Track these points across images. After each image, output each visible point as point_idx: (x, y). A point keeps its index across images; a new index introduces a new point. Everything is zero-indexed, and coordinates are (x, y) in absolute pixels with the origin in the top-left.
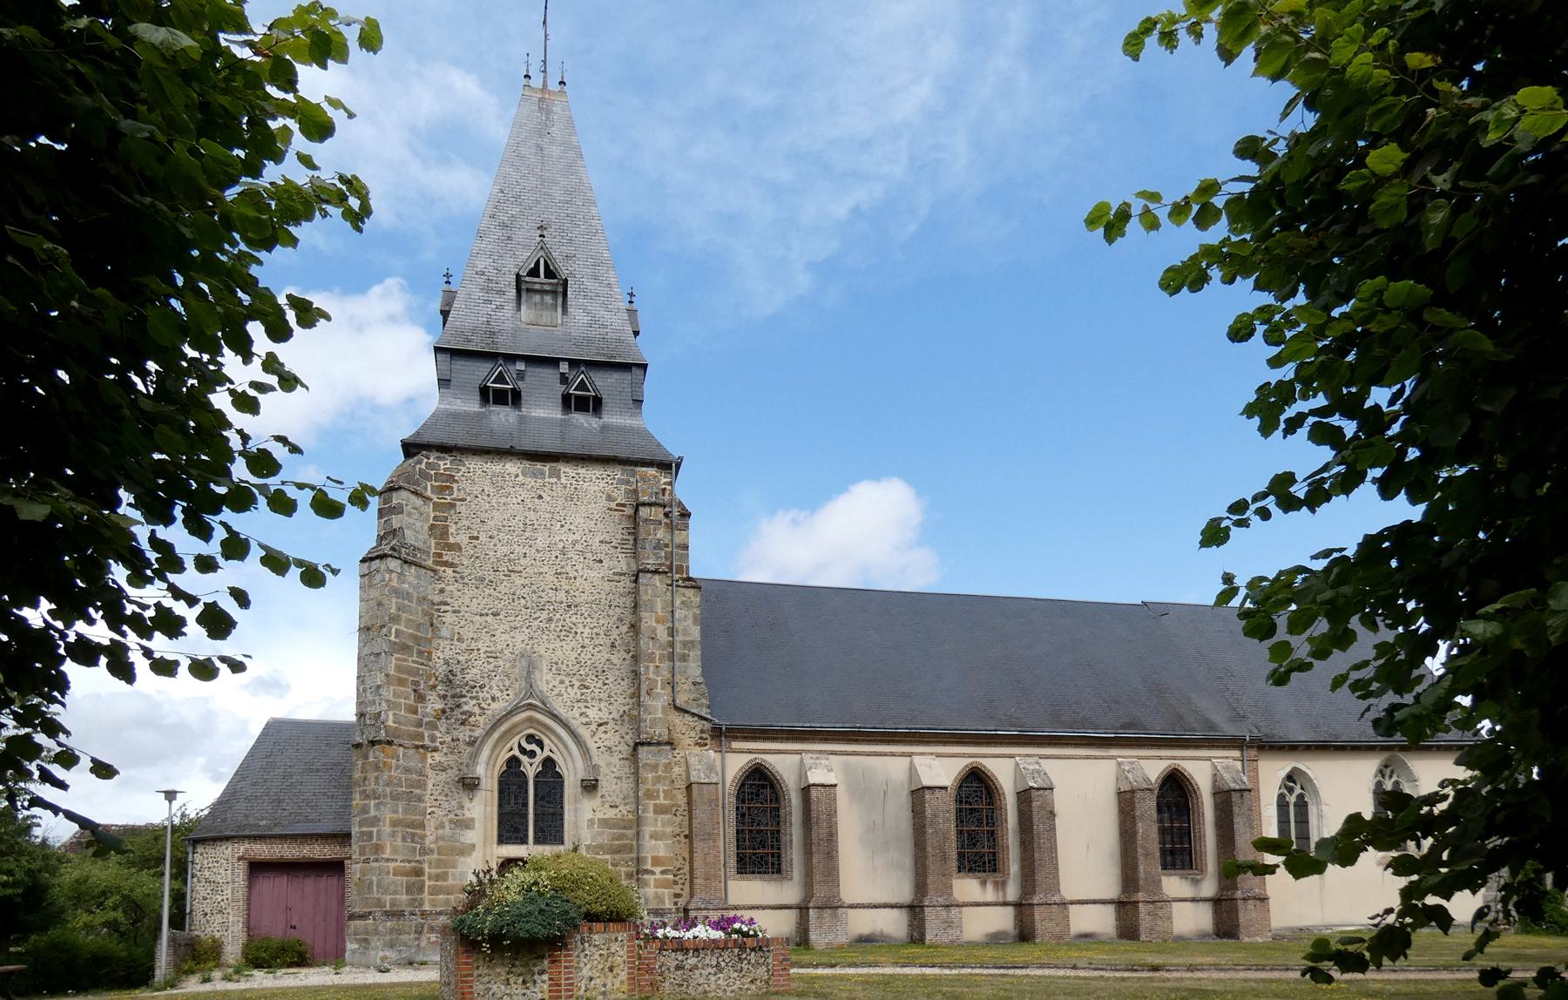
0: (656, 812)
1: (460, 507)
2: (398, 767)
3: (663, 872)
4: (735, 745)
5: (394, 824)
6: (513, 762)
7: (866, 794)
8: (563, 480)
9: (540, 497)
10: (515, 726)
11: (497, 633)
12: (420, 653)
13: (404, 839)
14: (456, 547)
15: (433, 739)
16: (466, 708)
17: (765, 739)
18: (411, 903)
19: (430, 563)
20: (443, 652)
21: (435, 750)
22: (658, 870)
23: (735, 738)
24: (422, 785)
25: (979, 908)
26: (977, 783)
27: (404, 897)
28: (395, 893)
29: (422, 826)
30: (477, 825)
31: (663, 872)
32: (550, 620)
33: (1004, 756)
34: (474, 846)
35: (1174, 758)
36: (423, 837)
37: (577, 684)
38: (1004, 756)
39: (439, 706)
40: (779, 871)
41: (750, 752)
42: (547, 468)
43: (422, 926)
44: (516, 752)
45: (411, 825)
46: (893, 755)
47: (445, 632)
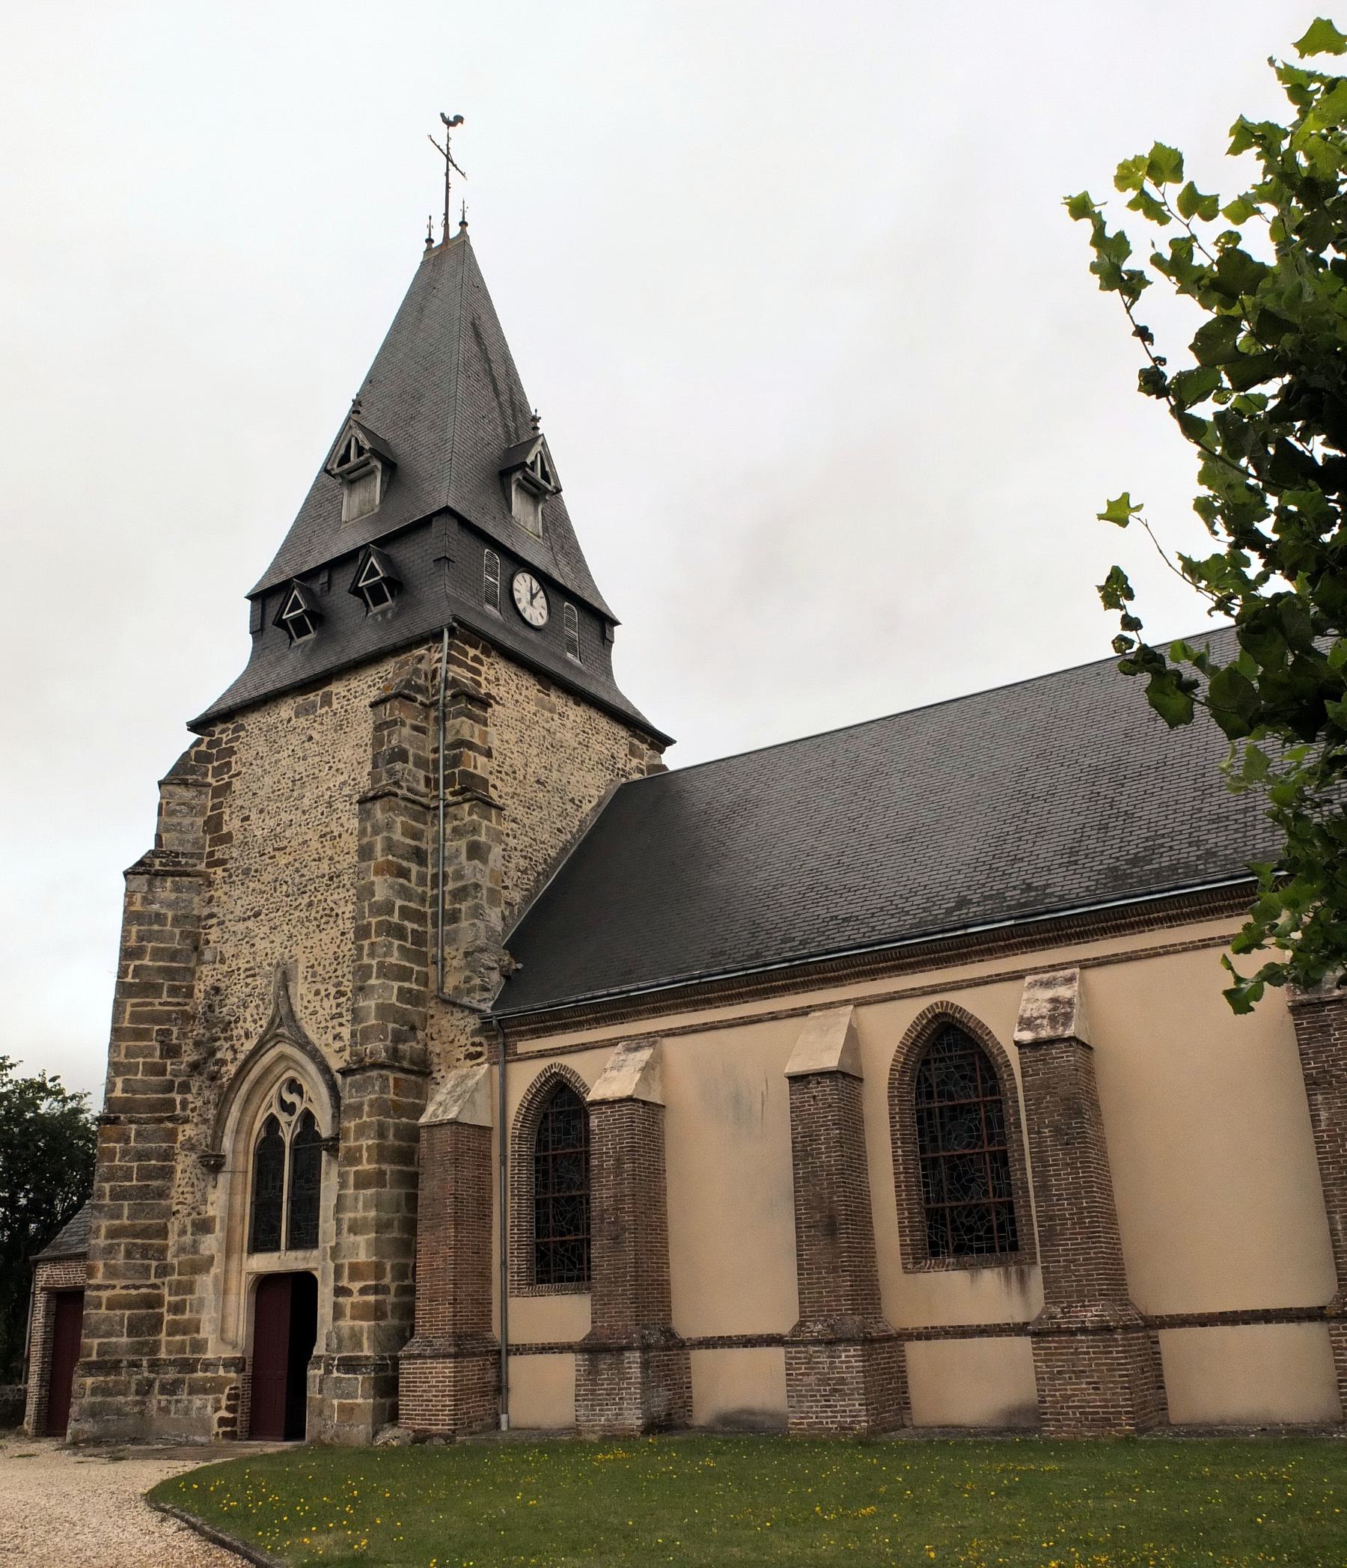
0: (357, 1187)
1: (237, 784)
2: (125, 1153)
3: (363, 1291)
4: (524, 1046)
5: (113, 1233)
6: (272, 1123)
7: (722, 1099)
8: (335, 706)
9: (310, 738)
10: (267, 1071)
11: (257, 941)
12: (174, 991)
13: (129, 1255)
14: (228, 838)
15: (184, 1104)
16: (219, 1055)
17: (1118, 930)
18: (137, 1348)
19: (202, 867)
20: (206, 977)
21: (186, 1121)
22: (356, 1286)
23: (521, 1035)
24: (167, 1173)
25: (973, 1344)
26: (948, 1048)
27: (125, 1339)
28: (109, 1334)
29: (163, 1232)
30: (218, 1227)
31: (363, 1291)
32: (310, 904)
33: (1000, 978)
34: (212, 1258)
35: (934, 990)
36: (162, 1251)
37: (333, 991)
38: (1000, 978)
39: (194, 1057)
40: (1014, 1247)
41: (542, 1054)
42: (314, 697)
43: (150, 1383)
44: (275, 1110)
45: (145, 1232)
46: (774, 1017)
47: (208, 956)
